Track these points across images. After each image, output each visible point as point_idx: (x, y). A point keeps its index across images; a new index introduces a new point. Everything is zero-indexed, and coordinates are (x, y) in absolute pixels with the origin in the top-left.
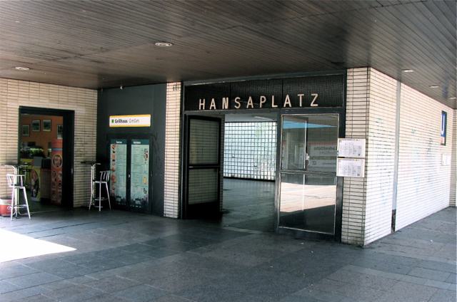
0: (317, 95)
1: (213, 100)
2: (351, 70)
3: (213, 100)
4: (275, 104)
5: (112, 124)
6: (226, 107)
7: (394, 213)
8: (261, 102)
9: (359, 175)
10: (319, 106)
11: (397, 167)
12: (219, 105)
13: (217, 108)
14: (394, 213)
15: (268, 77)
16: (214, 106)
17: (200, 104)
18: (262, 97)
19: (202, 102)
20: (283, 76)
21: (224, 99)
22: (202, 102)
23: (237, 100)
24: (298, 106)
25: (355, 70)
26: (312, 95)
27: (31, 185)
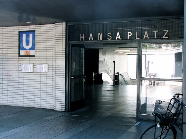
8: (128, 36)
18: (128, 33)
24: (98, 40)
26: (154, 31)
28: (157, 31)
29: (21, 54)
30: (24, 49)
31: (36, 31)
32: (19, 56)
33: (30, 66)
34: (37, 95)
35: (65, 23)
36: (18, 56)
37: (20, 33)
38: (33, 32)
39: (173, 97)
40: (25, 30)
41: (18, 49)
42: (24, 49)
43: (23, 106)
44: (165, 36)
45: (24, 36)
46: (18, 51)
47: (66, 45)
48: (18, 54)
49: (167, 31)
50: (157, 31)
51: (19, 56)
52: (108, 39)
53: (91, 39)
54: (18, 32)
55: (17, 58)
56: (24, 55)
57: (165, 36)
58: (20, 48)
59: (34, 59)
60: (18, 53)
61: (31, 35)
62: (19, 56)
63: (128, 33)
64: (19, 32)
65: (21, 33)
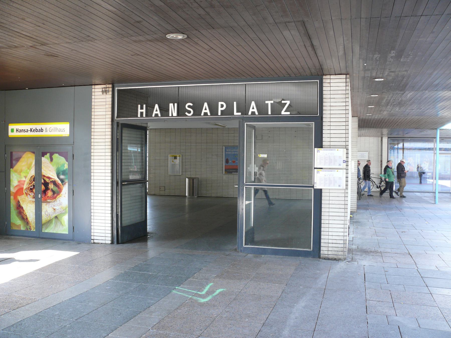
1: (157, 106)
2: (328, 77)
3: (157, 106)
4: (237, 112)
5: (11, 134)
6: (175, 114)
8: (220, 109)
9: (339, 186)
17: (140, 111)
18: (220, 103)
21: (171, 105)
23: (189, 106)
25: (332, 77)
44: (286, 111)
50: (272, 102)
53: (156, 115)
57: (286, 111)
63: (220, 103)
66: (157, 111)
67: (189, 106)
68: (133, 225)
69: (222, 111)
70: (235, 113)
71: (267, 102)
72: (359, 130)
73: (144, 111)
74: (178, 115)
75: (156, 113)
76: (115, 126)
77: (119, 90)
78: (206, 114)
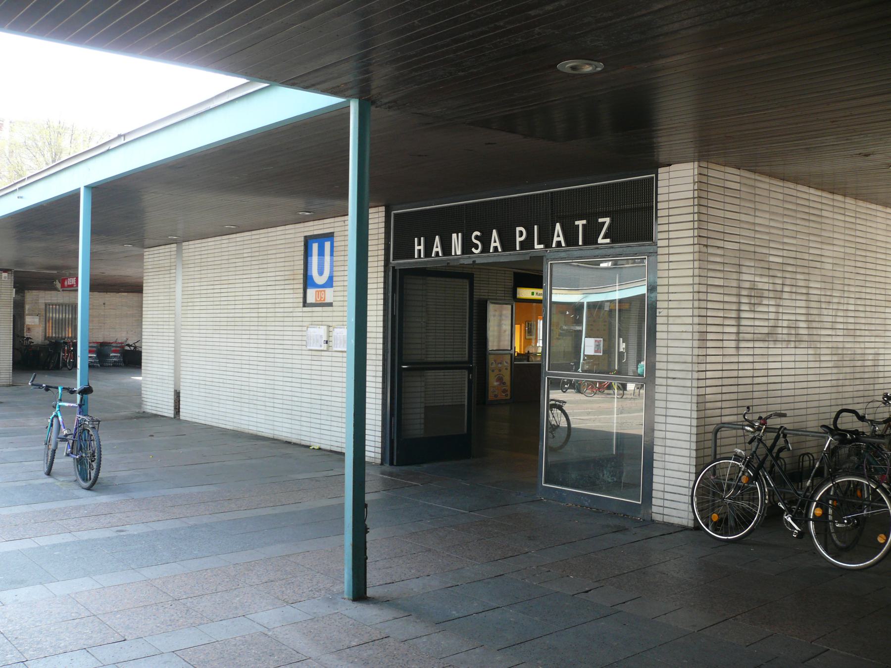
0: (607, 220)
3: (494, 232)
4: (539, 243)
6: (459, 252)
7: (177, 395)
8: (519, 239)
10: (613, 242)
11: (177, 352)
12: (546, 239)
13: (444, 254)
14: (177, 395)
15: (112, 146)
16: (561, 239)
17: (417, 248)
18: (518, 229)
19: (419, 244)
20: (122, 141)
21: (454, 236)
22: (419, 244)
23: (477, 238)
24: (515, 250)
26: (601, 220)
27: (790, 511)
28: (584, 222)
29: (309, 300)
30: (316, 286)
31: (335, 234)
32: (304, 306)
33: (322, 331)
34: (673, 451)
35: (383, 209)
36: (301, 305)
37: (308, 241)
38: (330, 236)
39: (830, 423)
40: (316, 233)
41: (301, 286)
42: (316, 286)
43: (255, 433)
44: (603, 238)
45: (315, 247)
46: (302, 291)
47: (385, 272)
48: (301, 300)
49: (607, 220)
50: (584, 222)
51: (304, 306)
52: (473, 250)
53: (559, 244)
54: (303, 239)
55: (297, 310)
56: (313, 301)
57: (603, 238)
58: (307, 282)
59: (330, 314)
60: (302, 295)
61: (327, 245)
62: (305, 304)
63: (518, 229)
64: (305, 237)
65: (310, 241)
66: (558, 236)
67: (477, 238)
68: (92, 208)
69: (521, 242)
70: (537, 246)
71: (577, 223)
72: (142, 283)
73: (422, 247)
74: (463, 253)
75: (558, 239)
76: (624, 287)
77: (395, 214)
78: (496, 248)
